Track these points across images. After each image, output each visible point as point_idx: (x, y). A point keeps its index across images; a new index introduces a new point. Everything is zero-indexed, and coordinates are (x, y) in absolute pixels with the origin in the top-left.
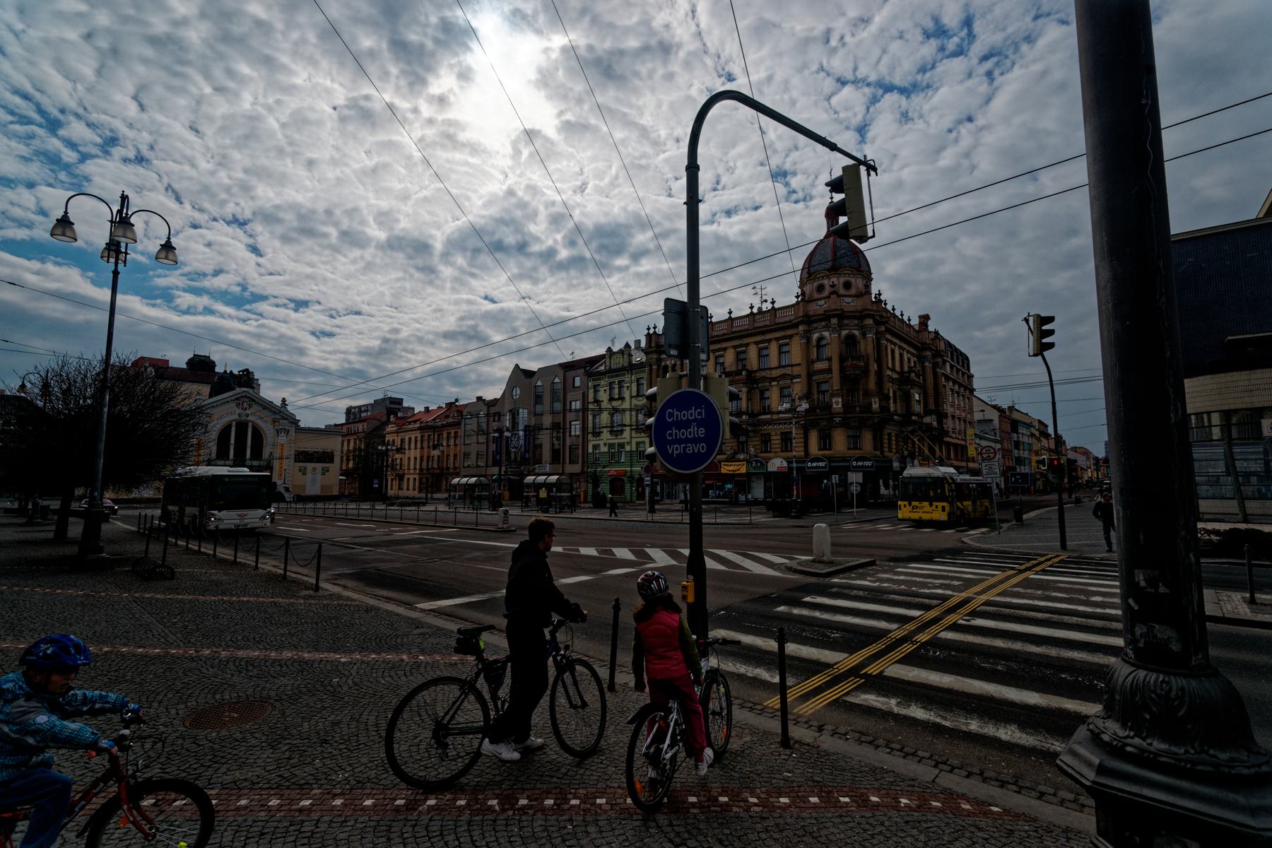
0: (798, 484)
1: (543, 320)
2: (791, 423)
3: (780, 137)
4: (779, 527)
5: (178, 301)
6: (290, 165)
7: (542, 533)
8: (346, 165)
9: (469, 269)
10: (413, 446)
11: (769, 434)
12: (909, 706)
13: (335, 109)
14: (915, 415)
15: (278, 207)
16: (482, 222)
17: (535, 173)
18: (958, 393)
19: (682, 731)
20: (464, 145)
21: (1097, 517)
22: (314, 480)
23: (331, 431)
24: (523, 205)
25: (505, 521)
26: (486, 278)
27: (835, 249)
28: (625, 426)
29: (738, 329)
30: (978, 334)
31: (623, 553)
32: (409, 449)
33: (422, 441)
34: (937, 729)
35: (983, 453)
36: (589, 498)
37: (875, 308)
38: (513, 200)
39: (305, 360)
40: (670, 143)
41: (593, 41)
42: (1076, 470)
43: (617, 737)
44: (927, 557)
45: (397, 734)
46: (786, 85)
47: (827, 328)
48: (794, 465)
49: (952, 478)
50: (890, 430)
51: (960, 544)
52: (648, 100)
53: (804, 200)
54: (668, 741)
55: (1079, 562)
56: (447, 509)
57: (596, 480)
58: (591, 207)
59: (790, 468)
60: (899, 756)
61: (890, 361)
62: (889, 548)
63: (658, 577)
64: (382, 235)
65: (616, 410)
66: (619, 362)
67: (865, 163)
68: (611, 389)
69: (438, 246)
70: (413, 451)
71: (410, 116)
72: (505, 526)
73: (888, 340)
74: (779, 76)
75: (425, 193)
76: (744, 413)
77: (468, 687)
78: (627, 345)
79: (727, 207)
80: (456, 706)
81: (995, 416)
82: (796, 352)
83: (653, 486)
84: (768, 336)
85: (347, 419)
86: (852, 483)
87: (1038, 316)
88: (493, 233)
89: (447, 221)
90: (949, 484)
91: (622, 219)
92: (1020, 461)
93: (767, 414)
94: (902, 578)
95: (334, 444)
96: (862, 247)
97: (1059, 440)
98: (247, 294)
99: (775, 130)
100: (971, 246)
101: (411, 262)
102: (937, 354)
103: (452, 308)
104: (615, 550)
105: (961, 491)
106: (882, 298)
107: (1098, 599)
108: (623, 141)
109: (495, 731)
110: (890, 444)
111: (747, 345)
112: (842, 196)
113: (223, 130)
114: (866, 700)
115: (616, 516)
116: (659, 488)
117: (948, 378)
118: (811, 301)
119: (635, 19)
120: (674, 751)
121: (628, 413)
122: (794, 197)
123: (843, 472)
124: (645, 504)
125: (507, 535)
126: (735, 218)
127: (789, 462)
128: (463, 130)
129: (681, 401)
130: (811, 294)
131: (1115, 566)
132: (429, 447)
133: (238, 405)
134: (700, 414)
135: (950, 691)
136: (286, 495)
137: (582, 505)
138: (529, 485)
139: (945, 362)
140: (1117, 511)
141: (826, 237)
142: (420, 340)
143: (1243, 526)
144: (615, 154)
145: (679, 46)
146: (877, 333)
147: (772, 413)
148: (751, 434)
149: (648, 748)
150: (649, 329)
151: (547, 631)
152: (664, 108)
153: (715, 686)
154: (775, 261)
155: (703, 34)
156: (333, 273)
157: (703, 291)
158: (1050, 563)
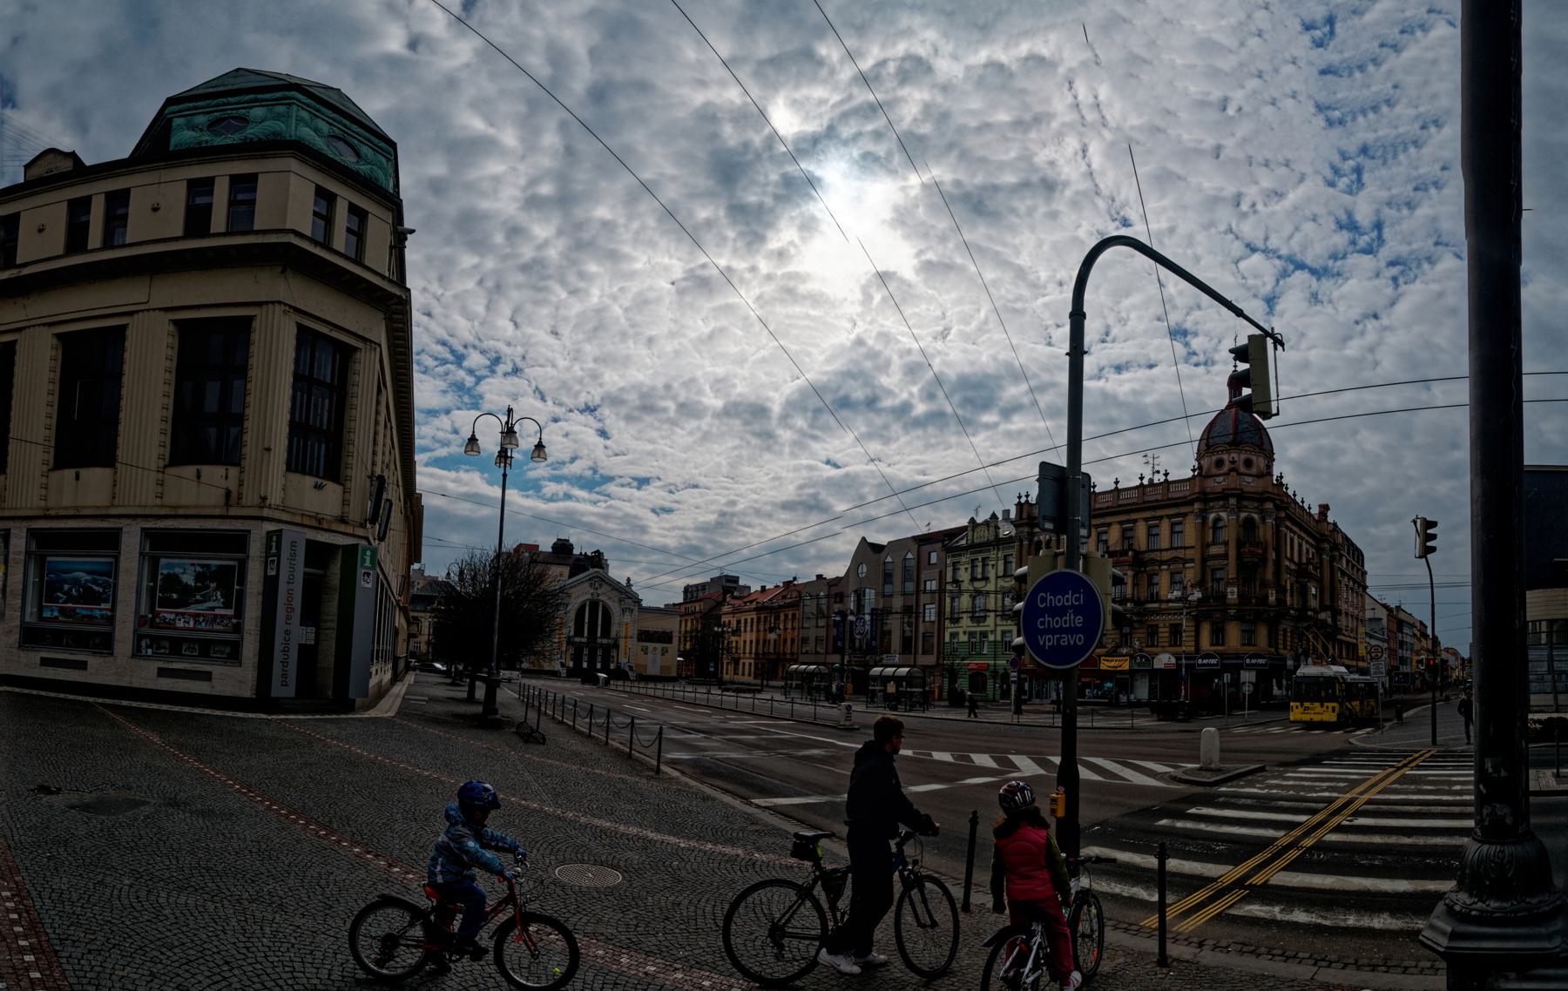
0: (1186, 683)
1: (895, 485)
2: (1182, 614)
3: (1181, 293)
4: (1164, 732)
5: (545, 490)
6: (632, 346)
7: (889, 733)
8: (684, 336)
9: (810, 432)
10: (749, 629)
11: (1157, 626)
12: (1292, 911)
13: (673, 283)
14: (1311, 610)
15: (622, 389)
16: (825, 378)
17: (888, 319)
18: (1352, 589)
19: (1046, 955)
20: (805, 297)
21: (1461, 714)
22: (656, 659)
23: (669, 610)
24: (873, 355)
25: (848, 718)
26: (828, 440)
27: (1237, 422)
28: (989, 611)
29: (1125, 502)
30: (1373, 530)
31: (983, 760)
32: (745, 631)
33: (758, 622)
34: (1317, 929)
35: (1374, 655)
36: (945, 695)
37: (1276, 491)
38: (863, 350)
39: (646, 538)
40: (1051, 287)
41: (961, 175)
42: (1447, 670)
43: (971, 960)
44: (1315, 760)
45: (733, 927)
46: (1190, 241)
47: (1224, 508)
48: (1184, 661)
49: (1342, 678)
50: (1286, 625)
51: (1347, 745)
52: (1026, 239)
53: (1206, 364)
54: (1029, 965)
55: (1446, 756)
56: (783, 698)
57: (953, 674)
58: (955, 355)
59: (1179, 666)
60: (1280, 961)
61: (1289, 551)
62: (1280, 752)
63: (1023, 789)
64: (718, 403)
65: (978, 592)
66: (983, 535)
67: (1272, 336)
68: (974, 567)
69: (776, 409)
70: (748, 634)
71: (747, 275)
72: (847, 723)
73: (1287, 527)
74: (1182, 229)
75: (763, 353)
76: (1127, 600)
77: (805, 893)
78: (994, 516)
79: (1117, 362)
80: (792, 911)
81: (1383, 614)
82: (1190, 533)
83: (1020, 682)
84: (1160, 513)
85: (685, 599)
86: (1244, 683)
87: (1425, 519)
88: (839, 388)
89: (785, 381)
90: (1340, 684)
91: (991, 369)
92: (1403, 661)
93: (1155, 602)
94: (1291, 783)
95: (672, 625)
96: (1266, 423)
97: (1435, 641)
98: (597, 477)
99: (1176, 284)
100: (1371, 440)
101: (748, 428)
102: (1335, 547)
103: (791, 475)
104: (973, 756)
105: (1351, 691)
106: (1284, 481)
107: (1458, 787)
108: (995, 282)
109: (834, 941)
110: (1285, 641)
111: (1135, 521)
112: (1246, 366)
113: (577, 326)
114: (1250, 911)
115: (976, 716)
116: (1027, 685)
117: (1343, 573)
118: (1208, 476)
119: (1013, 154)
120: (1036, 975)
121: (992, 596)
122: (1195, 359)
123: (1236, 670)
124: (1010, 704)
125: (849, 734)
126: (1126, 375)
127: (1178, 659)
128: (804, 282)
129: (1056, 584)
130: (1209, 469)
131: (1471, 756)
132: (765, 630)
133: (591, 585)
134: (1077, 599)
135: (1331, 892)
136: (630, 673)
137: (936, 703)
138: (875, 678)
139: (1341, 556)
140: (1475, 707)
141: (1228, 407)
142: (758, 512)
143: (1555, 715)
144: (984, 296)
145: (1066, 184)
146: (1277, 519)
147: (1161, 602)
148: (1136, 625)
149: (1007, 971)
150: (1020, 497)
151: (893, 843)
152: (1046, 248)
153: (1086, 907)
154: (1171, 426)
155: (1095, 175)
156: (671, 447)
157: (1086, 455)
158: (1422, 758)
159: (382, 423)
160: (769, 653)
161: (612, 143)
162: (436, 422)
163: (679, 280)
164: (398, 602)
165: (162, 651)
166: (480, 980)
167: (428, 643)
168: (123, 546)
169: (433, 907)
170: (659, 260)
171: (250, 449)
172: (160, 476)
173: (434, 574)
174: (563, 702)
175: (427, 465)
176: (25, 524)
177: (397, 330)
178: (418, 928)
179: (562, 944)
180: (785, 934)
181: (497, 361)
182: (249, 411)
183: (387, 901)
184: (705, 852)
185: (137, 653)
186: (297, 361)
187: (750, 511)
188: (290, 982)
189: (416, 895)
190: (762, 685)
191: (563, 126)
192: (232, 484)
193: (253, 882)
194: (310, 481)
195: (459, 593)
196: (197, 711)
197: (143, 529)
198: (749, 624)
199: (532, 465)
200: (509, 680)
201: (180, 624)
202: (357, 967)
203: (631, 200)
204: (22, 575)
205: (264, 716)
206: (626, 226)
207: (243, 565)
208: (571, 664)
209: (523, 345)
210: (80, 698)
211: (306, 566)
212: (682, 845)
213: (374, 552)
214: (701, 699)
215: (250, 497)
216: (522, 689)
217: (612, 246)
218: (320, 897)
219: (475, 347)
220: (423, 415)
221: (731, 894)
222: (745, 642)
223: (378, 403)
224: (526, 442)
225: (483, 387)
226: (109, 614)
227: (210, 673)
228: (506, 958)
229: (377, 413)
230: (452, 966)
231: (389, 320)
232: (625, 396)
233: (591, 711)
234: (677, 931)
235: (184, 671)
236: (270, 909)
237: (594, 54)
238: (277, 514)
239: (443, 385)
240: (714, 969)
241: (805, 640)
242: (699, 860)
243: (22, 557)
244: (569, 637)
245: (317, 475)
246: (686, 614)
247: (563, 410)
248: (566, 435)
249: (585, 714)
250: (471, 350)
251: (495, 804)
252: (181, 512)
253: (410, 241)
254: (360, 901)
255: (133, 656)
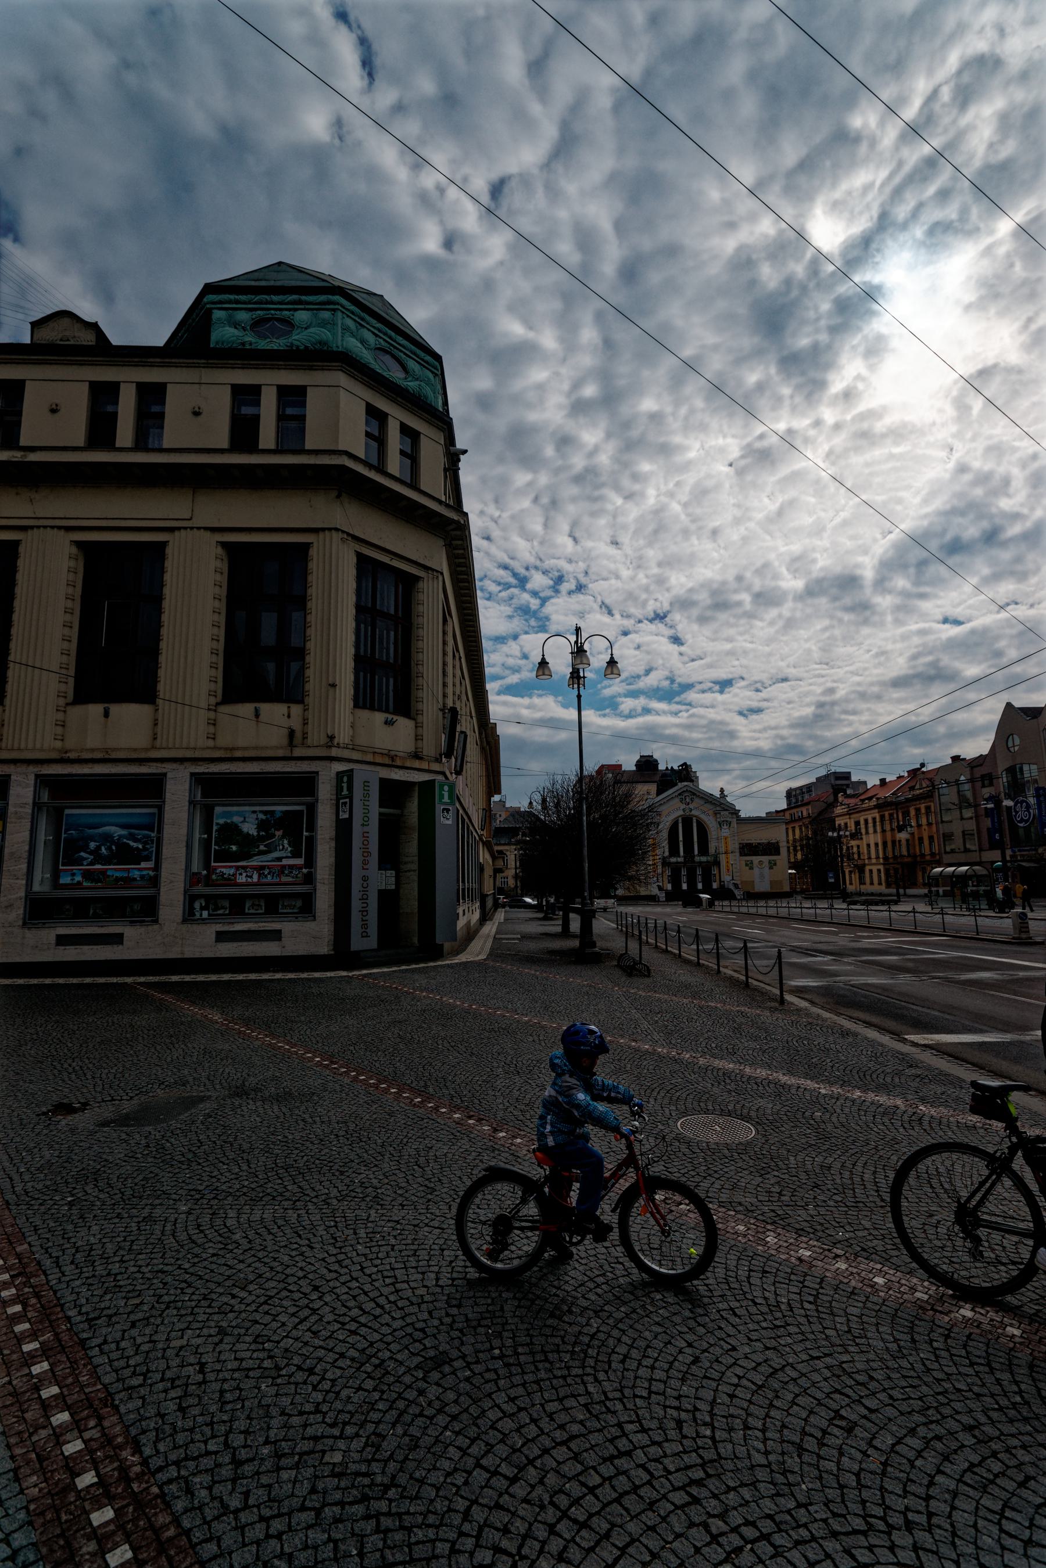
5: (622, 707)
6: (696, 542)
8: (750, 519)
10: (871, 830)
13: (731, 465)
15: (691, 590)
16: (925, 523)
20: (884, 436)
23: (773, 818)
24: (983, 478)
26: (942, 594)
32: (867, 833)
38: (967, 477)
39: (735, 743)
45: (904, 1203)
56: (929, 909)
64: (798, 584)
69: (868, 574)
71: (812, 433)
72: (1024, 936)
75: (843, 515)
77: (999, 1166)
80: (985, 1189)
85: (789, 804)
89: (875, 540)
95: (778, 834)
101: (837, 604)
103: (899, 646)
113: (637, 532)
132: (892, 830)
136: (736, 892)
159: (450, 654)
160: (902, 856)
161: (649, 324)
162: (505, 649)
163: (737, 460)
164: (480, 837)
165: (221, 912)
166: (606, 1267)
167: (516, 877)
168: (168, 795)
169: (546, 1177)
170: (713, 443)
171: (313, 685)
172: (212, 715)
173: (515, 804)
174: (665, 928)
175: (499, 693)
176: (33, 769)
177: (457, 557)
178: (532, 1204)
179: (694, 1217)
180: (978, 1223)
181: (560, 579)
182: (310, 645)
183: (496, 1175)
184: (853, 1101)
185: (189, 917)
186: (359, 592)
187: (853, 696)
188: (392, 1298)
189: (526, 1164)
190: (898, 895)
191: (599, 318)
192: (296, 724)
193: (342, 1173)
194: (379, 717)
195: (543, 822)
196: (266, 976)
197: (192, 774)
198: (870, 825)
199: (606, 682)
200: (605, 909)
201: (242, 879)
202: (468, 1264)
203: (676, 383)
204: (27, 834)
205: (344, 973)
206: (673, 414)
207: (312, 809)
208: (669, 887)
209: (584, 560)
210: (114, 980)
211: (380, 806)
212: (823, 1091)
213: (452, 787)
214: (823, 916)
215: (316, 736)
216: (619, 917)
217: (662, 439)
218: (420, 1180)
219: (536, 568)
220: (491, 643)
221: (894, 1158)
222: (868, 845)
223: (444, 633)
224: (598, 660)
225: (549, 609)
226: (151, 873)
227: (280, 931)
228: (634, 1236)
229: (445, 643)
230: (574, 1251)
231: (449, 547)
232: (695, 597)
233: (697, 936)
234: (831, 1203)
235: (249, 932)
236: (363, 1205)
237: (620, 226)
238: (346, 754)
239: (508, 610)
240: (886, 1260)
241: (948, 837)
242: (847, 1110)
243: (29, 810)
244: (664, 858)
245: (387, 711)
246: (793, 820)
247: (632, 621)
248: (638, 647)
249: (691, 940)
250: (533, 572)
251: (602, 1048)
252: (238, 754)
253: (464, 462)
254: (465, 1179)
255: (185, 921)
